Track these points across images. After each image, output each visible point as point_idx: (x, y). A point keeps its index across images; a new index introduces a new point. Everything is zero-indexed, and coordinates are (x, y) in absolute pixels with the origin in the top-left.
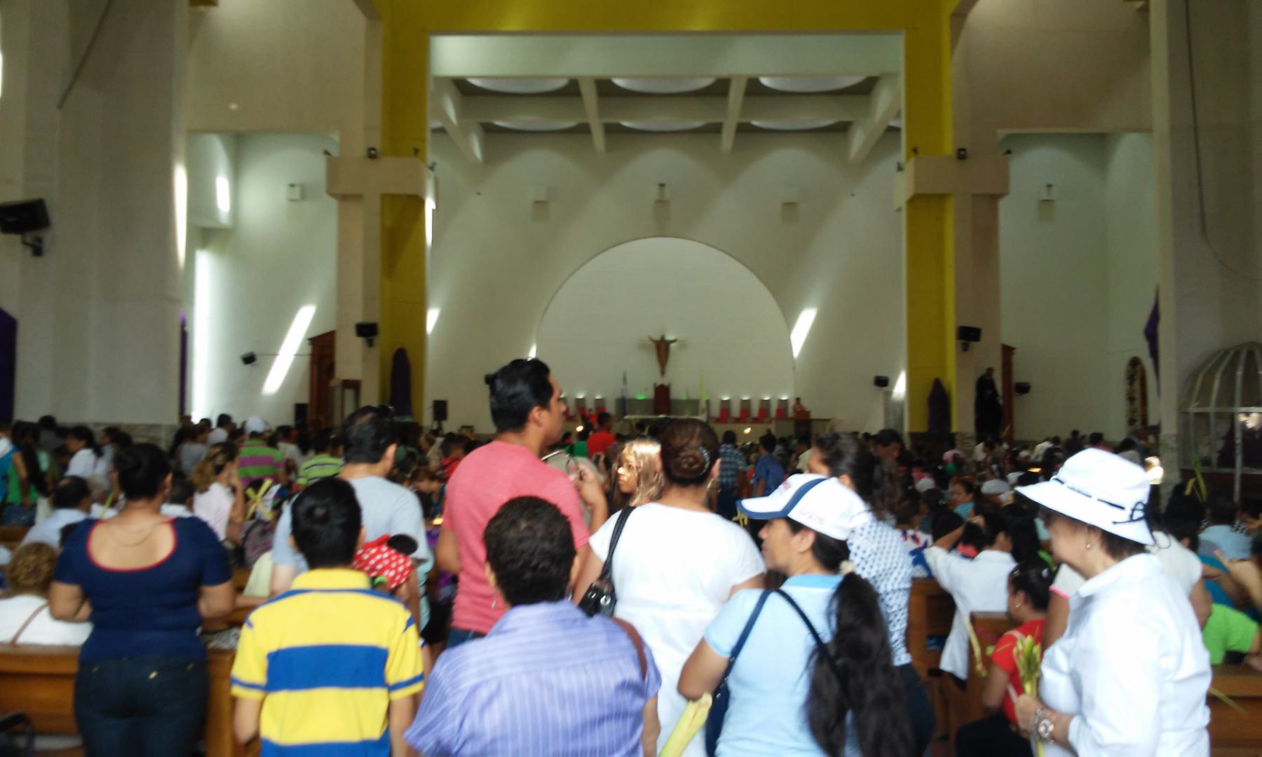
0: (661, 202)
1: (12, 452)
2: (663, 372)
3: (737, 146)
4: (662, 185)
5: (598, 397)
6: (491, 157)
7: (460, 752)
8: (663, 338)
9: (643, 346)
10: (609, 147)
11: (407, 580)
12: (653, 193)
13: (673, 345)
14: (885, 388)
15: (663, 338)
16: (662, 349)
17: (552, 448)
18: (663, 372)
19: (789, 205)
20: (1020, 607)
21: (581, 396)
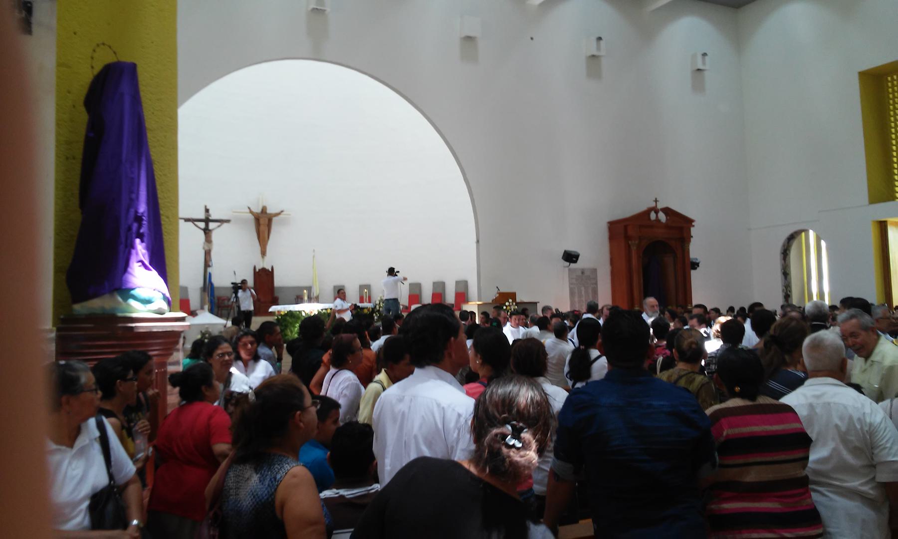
2: (263, 253)
8: (264, 210)
15: (264, 210)
18: (263, 253)
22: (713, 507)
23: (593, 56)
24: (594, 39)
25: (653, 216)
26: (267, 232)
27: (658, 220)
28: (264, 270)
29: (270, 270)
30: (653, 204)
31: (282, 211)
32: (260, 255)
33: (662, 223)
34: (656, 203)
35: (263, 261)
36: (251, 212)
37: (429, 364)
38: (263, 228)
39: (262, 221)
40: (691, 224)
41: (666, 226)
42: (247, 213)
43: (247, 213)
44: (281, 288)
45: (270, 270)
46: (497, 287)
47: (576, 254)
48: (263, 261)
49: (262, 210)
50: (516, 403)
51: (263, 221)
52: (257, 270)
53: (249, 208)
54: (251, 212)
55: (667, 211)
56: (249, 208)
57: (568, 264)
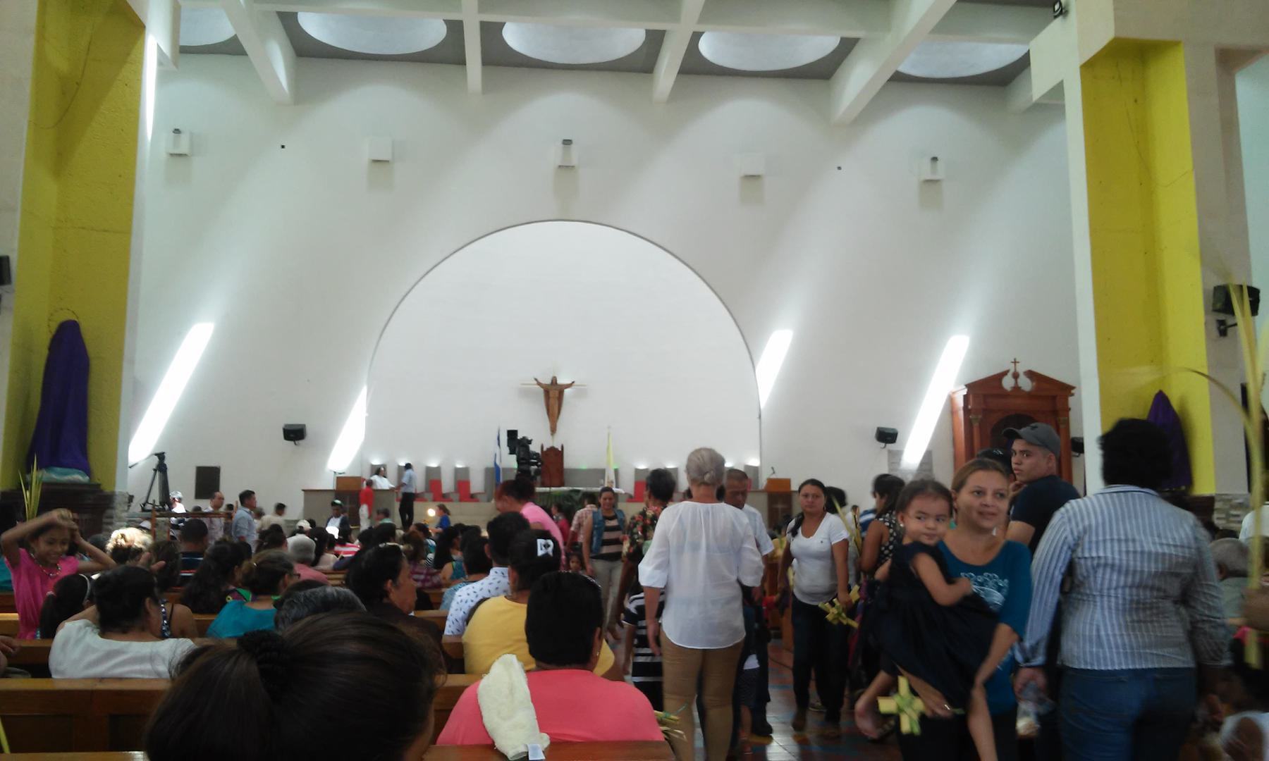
0: (565, 168)
1: (520, 510)
2: (553, 430)
3: (677, 92)
4: (567, 142)
5: (459, 466)
6: (303, 93)
7: (174, 613)
8: (554, 381)
9: (524, 393)
10: (488, 85)
11: (169, 623)
12: (555, 154)
13: (567, 391)
14: (889, 446)
15: (554, 381)
16: (553, 396)
17: (1196, 574)
18: (553, 430)
19: (752, 178)
20: (132, 523)
21: (434, 464)
22: (364, 391)
23: (928, 181)
24: (927, 161)
25: (1008, 383)
26: (557, 405)
27: (1017, 388)
28: (552, 449)
29: (560, 449)
30: (1011, 368)
31: (573, 382)
32: (549, 431)
33: (1006, 390)
34: (1015, 365)
35: (553, 438)
36: (539, 384)
37: (939, 690)
38: (554, 402)
39: (551, 394)
40: (1070, 392)
41: (1030, 395)
42: (534, 385)
43: (534, 385)
44: (567, 469)
45: (560, 449)
46: (773, 468)
47: (891, 432)
48: (553, 438)
49: (552, 381)
50: (660, 550)
51: (553, 394)
52: (545, 449)
53: (536, 380)
54: (539, 384)
55: (1031, 374)
56: (536, 380)
57: (883, 445)
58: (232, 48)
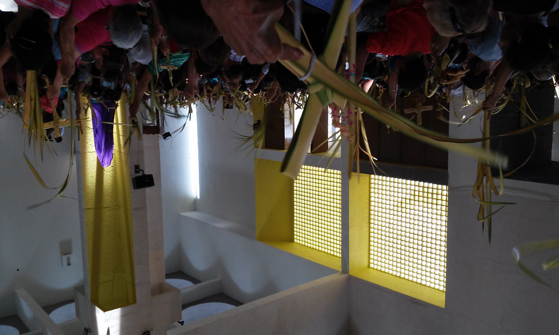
58: (49, 309)
